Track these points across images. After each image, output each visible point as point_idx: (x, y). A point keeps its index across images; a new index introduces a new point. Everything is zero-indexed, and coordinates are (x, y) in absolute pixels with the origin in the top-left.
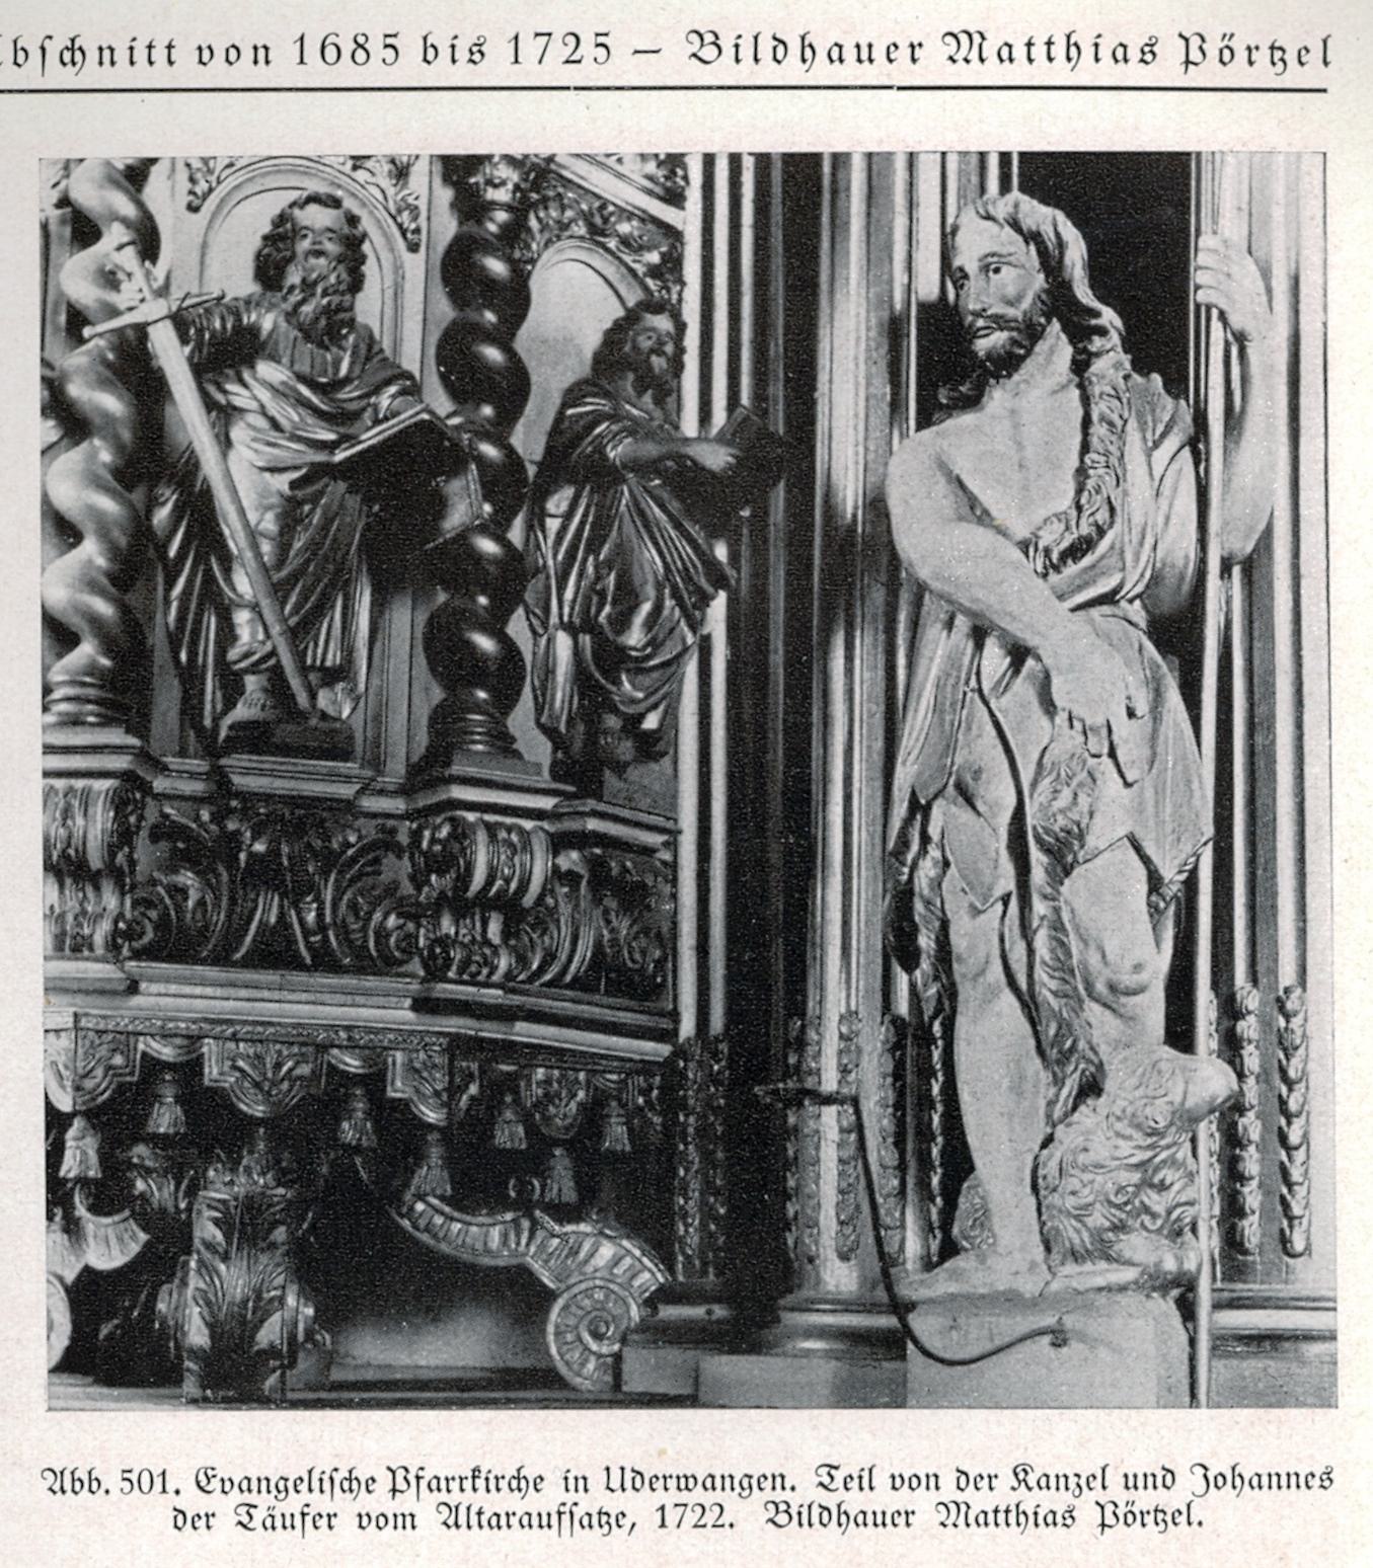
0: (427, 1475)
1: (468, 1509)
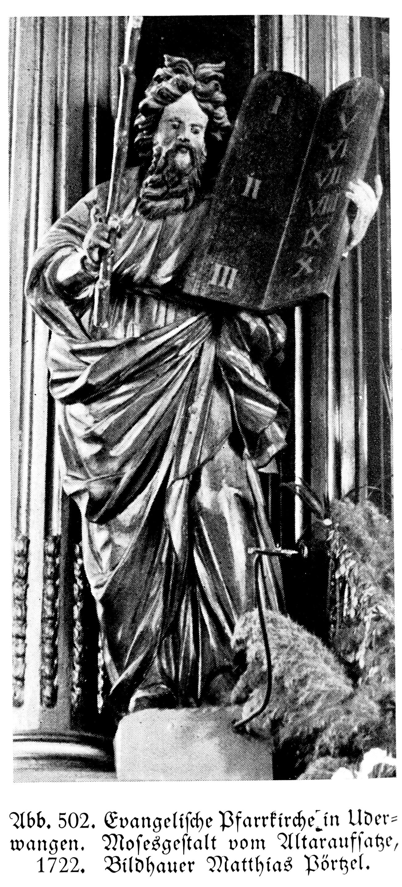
0: (243, 816)
1: (297, 836)
